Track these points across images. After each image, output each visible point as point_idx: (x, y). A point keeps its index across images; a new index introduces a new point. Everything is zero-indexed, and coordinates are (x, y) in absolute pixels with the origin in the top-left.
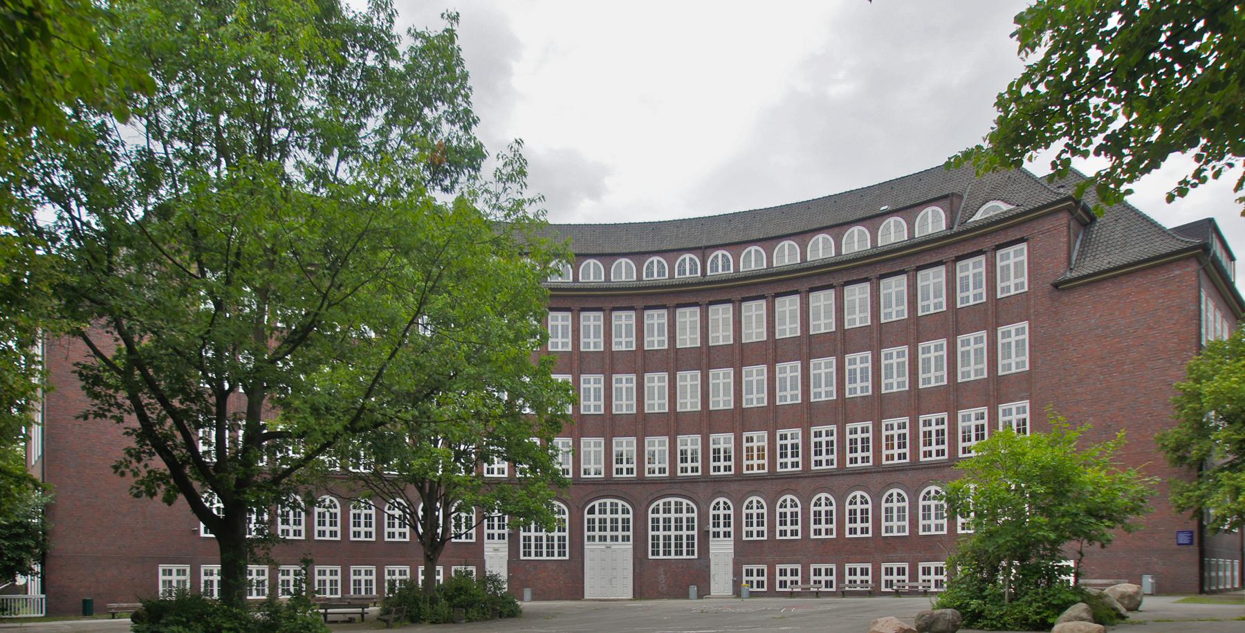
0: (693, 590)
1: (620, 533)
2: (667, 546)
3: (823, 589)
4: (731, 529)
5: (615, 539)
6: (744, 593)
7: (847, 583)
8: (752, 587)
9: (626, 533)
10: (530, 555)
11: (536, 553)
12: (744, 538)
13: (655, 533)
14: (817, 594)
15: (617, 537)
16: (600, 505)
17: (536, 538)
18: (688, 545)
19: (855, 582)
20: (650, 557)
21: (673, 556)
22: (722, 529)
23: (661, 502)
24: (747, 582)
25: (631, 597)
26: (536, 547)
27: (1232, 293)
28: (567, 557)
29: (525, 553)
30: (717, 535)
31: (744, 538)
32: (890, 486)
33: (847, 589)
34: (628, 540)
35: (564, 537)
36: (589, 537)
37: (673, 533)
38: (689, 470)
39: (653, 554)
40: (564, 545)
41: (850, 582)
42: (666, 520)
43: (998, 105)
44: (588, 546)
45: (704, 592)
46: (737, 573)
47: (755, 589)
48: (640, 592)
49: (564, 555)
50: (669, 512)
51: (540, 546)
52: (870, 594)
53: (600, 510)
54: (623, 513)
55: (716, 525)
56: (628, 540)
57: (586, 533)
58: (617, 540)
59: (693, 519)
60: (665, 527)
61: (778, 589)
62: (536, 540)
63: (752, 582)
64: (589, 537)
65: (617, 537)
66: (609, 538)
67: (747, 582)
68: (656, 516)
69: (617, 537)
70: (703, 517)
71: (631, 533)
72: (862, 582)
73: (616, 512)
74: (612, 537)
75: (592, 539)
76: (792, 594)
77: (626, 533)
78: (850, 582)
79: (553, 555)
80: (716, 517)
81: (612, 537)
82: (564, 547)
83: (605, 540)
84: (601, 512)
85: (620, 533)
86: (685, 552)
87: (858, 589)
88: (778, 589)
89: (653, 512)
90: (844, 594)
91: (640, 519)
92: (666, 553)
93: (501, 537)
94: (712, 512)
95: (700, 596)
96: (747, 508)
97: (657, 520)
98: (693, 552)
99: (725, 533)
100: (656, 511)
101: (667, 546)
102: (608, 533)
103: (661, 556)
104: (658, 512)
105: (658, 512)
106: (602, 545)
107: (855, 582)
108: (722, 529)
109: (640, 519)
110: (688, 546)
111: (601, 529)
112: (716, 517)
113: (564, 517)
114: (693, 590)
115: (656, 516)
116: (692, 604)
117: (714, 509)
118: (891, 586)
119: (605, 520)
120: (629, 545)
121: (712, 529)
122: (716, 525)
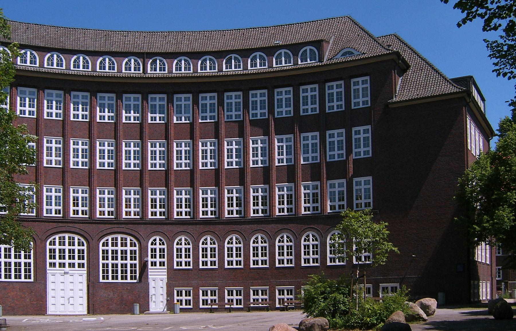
0: (137, 307)
1: (76, 261)
2: (18, 271)
3: (235, 306)
4: (165, 260)
5: (72, 265)
6: (178, 307)
7: (252, 301)
8: (181, 304)
9: (81, 261)
10: (20, 278)
11: (122, 277)
12: (175, 267)
13: (28, 261)
14: (230, 310)
15: (74, 264)
16: (113, 239)
17: (25, 264)
18: (122, 272)
19: (258, 300)
20: (101, 280)
21: (120, 280)
22: (158, 260)
23: (110, 238)
24: (178, 301)
25: (86, 313)
26: (122, 273)
27: (488, 126)
28: (32, 280)
29: (103, 277)
30: (154, 264)
31: (175, 267)
32: (304, 231)
33: (252, 305)
34: (83, 267)
35: (30, 263)
36: (50, 264)
37: (119, 262)
38: (106, 213)
39: (103, 279)
40: (30, 270)
41: (254, 300)
42: (61, 251)
43: (510, 106)
44: (50, 270)
45: (145, 308)
46: (170, 294)
47: (184, 306)
48: (92, 309)
49: (30, 278)
50: (126, 246)
51: (125, 272)
52: (267, 309)
53: (112, 244)
54: (131, 246)
55: (154, 256)
56: (83, 267)
57: (48, 261)
58: (74, 267)
59: (83, 250)
60: (113, 257)
61: (201, 306)
62: (113, 267)
63: (181, 301)
64: (50, 264)
65: (55, 264)
66: (67, 265)
67: (178, 301)
68: (105, 248)
69: (55, 264)
70: (143, 250)
71: (85, 261)
72: (262, 300)
73: (124, 244)
74: (70, 264)
75: (53, 265)
76: (211, 310)
77: (81, 261)
78: (254, 300)
79: (10, 278)
80: (154, 250)
81: (79, 264)
82: (30, 272)
83: (64, 267)
84: (61, 243)
85: (76, 261)
86: (120, 277)
87: (260, 305)
88: (201, 306)
89: (50, 244)
90: (249, 309)
91: (93, 251)
92: (124, 277)
93: (81, 266)
94: (150, 247)
95: (142, 312)
96: (177, 244)
97: (53, 251)
98: (30, 276)
99: (160, 263)
100: (106, 244)
101: (18, 271)
102: (67, 261)
103: (110, 280)
104: (107, 246)
105: (107, 246)
106: (62, 270)
107: (258, 300)
108: (158, 260)
109: (93, 251)
110: (26, 271)
111: (71, 257)
112: (154, 250)
113: (332, 256)
114: (137, 307)
115: (105, 248)
116: (138, 318)
117: (152, 244)
118: (283, 303)
119: (74, 250)
120: (84, 271)
121: (150, 260)
122: (154, 256)
